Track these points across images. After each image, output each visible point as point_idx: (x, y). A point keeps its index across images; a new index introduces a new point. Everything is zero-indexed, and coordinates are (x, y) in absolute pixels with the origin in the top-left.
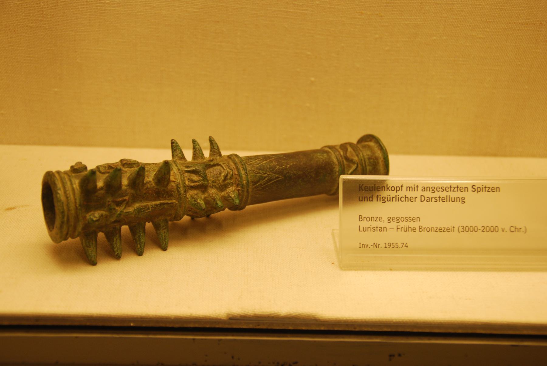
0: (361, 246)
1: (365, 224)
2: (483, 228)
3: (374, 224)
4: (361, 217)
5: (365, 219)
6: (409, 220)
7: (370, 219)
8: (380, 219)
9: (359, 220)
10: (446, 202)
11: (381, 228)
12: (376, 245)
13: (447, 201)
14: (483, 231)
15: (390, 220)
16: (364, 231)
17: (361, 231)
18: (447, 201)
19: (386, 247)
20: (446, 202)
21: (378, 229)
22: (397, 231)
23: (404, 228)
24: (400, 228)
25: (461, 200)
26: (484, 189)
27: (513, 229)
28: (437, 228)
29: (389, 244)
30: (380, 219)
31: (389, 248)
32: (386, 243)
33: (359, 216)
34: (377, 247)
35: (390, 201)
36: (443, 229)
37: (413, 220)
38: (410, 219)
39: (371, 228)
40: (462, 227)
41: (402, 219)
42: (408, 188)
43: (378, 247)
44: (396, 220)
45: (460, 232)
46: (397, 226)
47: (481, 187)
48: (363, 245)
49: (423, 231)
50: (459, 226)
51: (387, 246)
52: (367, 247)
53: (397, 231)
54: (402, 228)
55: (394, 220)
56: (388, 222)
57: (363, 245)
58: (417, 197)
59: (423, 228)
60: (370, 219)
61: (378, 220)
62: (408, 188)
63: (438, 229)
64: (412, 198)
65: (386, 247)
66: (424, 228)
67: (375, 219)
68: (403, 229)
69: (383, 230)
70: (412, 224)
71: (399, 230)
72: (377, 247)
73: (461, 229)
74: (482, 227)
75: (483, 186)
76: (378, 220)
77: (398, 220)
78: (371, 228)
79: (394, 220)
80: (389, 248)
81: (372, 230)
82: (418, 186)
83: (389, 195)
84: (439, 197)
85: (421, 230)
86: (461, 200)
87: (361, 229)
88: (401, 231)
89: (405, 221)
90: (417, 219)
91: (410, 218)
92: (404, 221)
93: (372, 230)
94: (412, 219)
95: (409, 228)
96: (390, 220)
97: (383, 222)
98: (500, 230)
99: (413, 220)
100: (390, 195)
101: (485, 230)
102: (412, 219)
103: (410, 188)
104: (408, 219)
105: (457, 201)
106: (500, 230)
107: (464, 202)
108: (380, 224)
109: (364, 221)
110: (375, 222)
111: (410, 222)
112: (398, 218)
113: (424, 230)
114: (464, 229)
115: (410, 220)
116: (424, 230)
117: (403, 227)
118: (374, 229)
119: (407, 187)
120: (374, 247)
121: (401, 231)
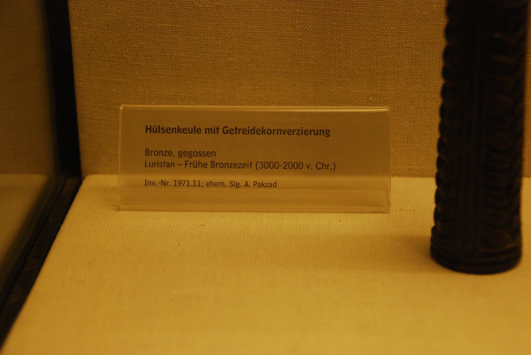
0: (147, 184)
1: (153, 159)
2: (285, 164)
3: (161, 159)
4: (147, 150)
5: (153, 153)
6: (203, 154)
7: (223, 165)
8: (170, 153)
9: (146, 154)
10: (292, 135)
11: (168, 164)
12: (163, 183)
13: (173, 133)
14: (285, 167)
15: (180, 155)
16: (150, 167)
17: (148, 167)
18: (173, 133)
19: (175, 184)
20: (292, 135)
21: (166, 164)
22: (185, 167)
23: (194, 163)
24: (189, 163)
25: (325, 133)
26: (216, 130)
27: (319, 166)
28: (167, 151)
29: (180, 182)
30: (170, 153)
31: (179, 185)
32: (175, 181)
33: (211, 162)
34: (165, 185)
35: (317, 134)
36: (239, 165)
37: (208, 154)
38: (204, 154)
39: (158, 163)
40: (261, 163)
41: (195, 154)
42: (207, 130)
43: (167, 185)
44: (188, 154)
45: (258, 168)
46: (186, 161)
47: (213, 128)
48: (149, 182)
49: (150, 155)
50: (257, 162)
51: (177, 184)
52: (154, 185)
53: (185, 167)
54: (192, 163)
55: (185, 155)
56: (179, 157)
57: (149, 182)
58: (329, 165)
59: (150, 152)
60: (223, 165)
61: (232, 166)
62: (207, 130)
63: (242, 165)
64: (306, 131)
65: (175, 184)
66: (217, 164)
67: (230, 165)
68: (192, 165)
69: (170, 166)
70: (203, 160)
71: (188, 166)
72: (165, 185)
73: (259, 165)
74: (284, 163)
75: (214, 127)
76: (232, 166)
77: (190, 154)
78: (158, 163)
79: (185, 155)
80: (179, 185)
81: (159, 165)
82: (219, 128)
83: (155, 125)
84: (236, 128)
85: (213, 166)
86: (325, 133)
87: (148, 165)
88: (190, 167)
89: (199, 156)
90: (212, 153)
91: (204, 153)
92: (198, 156)
93: (159, 165)
94: (206, 153)
95: (199, 163)
96: (180, 155)
97: (173, 156)
98: (305, 166)
99: (208, 154)
100: (156, 126)
101: (287, 167)
102: (206, 153)
103: (209, 129)
104: (202, 153)
105: (320, 134)
106: (305, 166)
107: (329, 135)
108: (168, 159)
109: (151, 155)
110: (163, 156)
111: (204, 157)
112: (190, 153)
113: (151, 153)
114: (263, 165)
115: (204, 155)
116: (151, 153)
117: (193, 162)
118: (161, 165)
119: (206, 129)
120: (162, 185)
121: (190, 167)
